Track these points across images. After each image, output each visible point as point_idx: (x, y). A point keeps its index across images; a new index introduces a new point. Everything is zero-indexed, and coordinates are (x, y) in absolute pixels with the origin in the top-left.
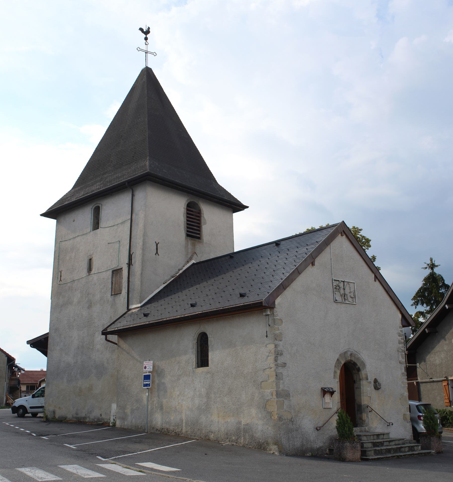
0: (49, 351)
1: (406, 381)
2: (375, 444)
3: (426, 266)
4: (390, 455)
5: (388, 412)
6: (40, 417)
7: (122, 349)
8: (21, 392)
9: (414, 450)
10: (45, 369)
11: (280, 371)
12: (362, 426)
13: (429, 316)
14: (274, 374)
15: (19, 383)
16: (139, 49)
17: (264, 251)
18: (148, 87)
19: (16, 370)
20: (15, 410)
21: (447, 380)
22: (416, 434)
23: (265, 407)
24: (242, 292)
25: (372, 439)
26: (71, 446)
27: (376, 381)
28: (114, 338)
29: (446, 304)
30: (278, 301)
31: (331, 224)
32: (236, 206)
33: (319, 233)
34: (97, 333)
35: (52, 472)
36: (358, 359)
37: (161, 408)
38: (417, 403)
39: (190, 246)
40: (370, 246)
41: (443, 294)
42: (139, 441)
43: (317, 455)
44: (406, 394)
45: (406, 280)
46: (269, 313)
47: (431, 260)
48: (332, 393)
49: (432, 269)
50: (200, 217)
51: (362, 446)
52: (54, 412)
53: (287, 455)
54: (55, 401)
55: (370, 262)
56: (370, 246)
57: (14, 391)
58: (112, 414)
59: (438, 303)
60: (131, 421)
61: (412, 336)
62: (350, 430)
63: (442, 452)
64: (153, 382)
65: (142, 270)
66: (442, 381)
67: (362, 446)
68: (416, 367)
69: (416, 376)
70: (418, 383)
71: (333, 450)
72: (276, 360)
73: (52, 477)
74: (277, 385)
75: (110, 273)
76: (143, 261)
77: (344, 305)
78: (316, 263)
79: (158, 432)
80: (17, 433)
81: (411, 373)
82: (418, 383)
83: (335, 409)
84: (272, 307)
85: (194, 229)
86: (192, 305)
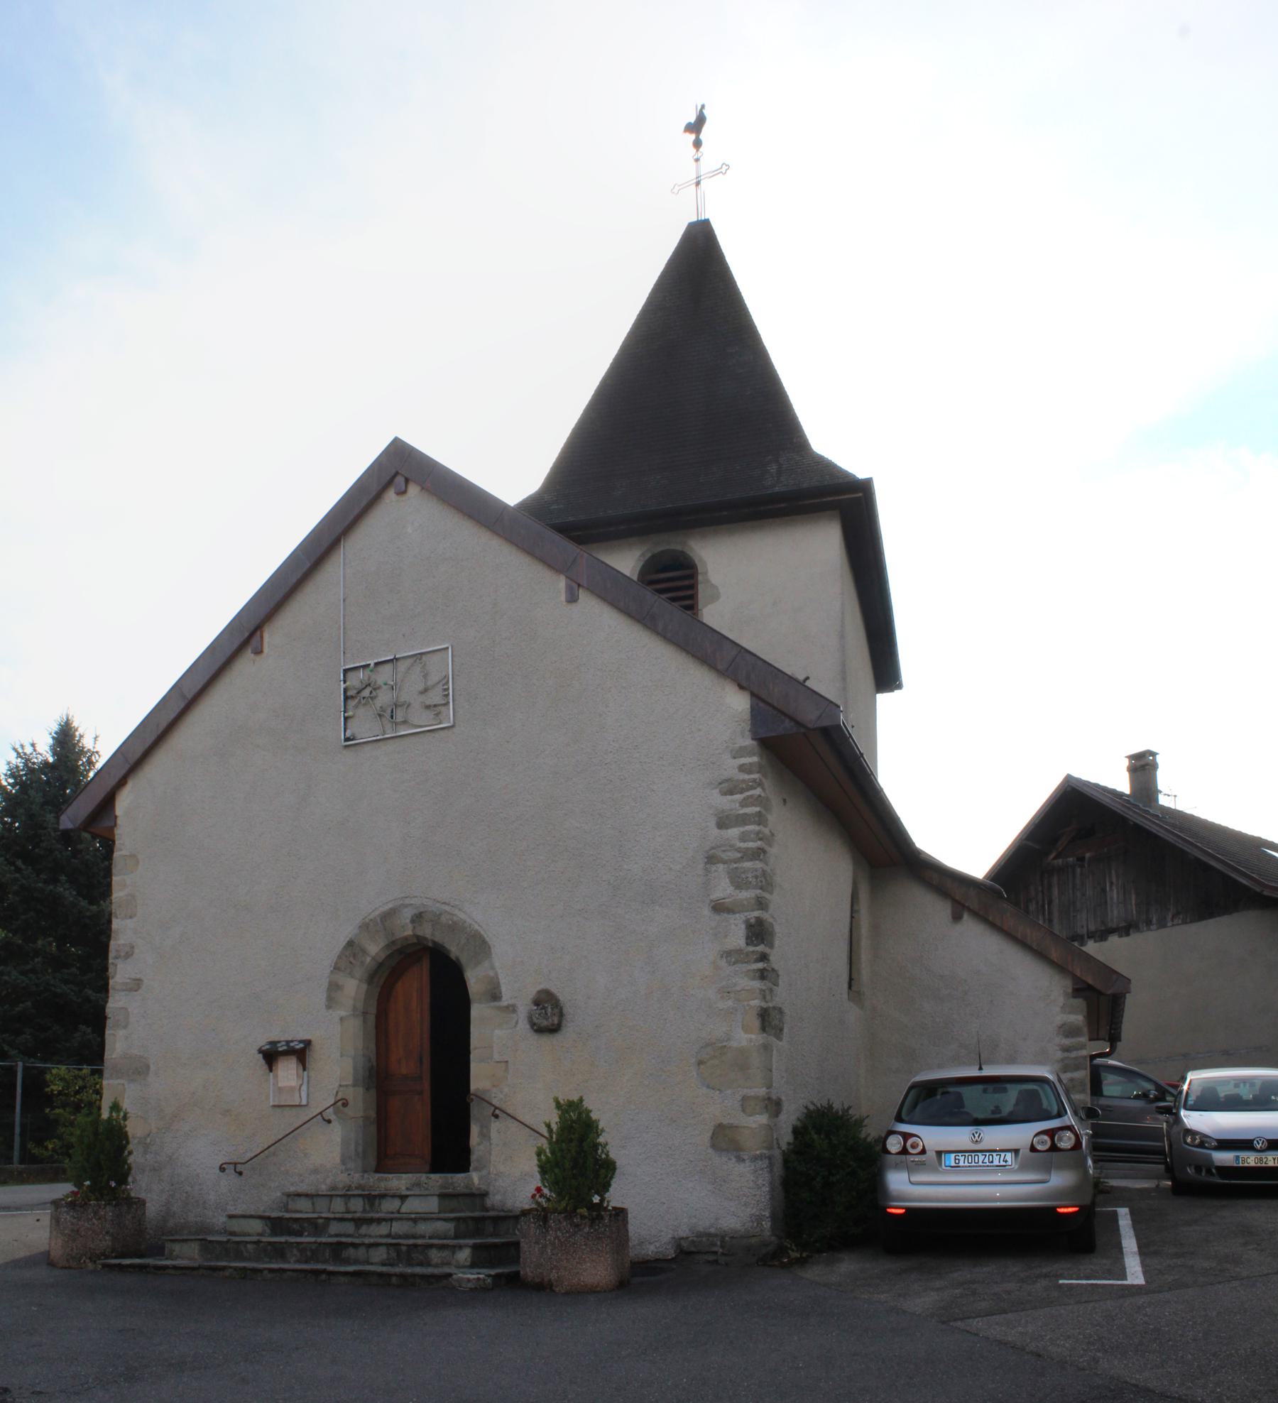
11: (120, 1004)
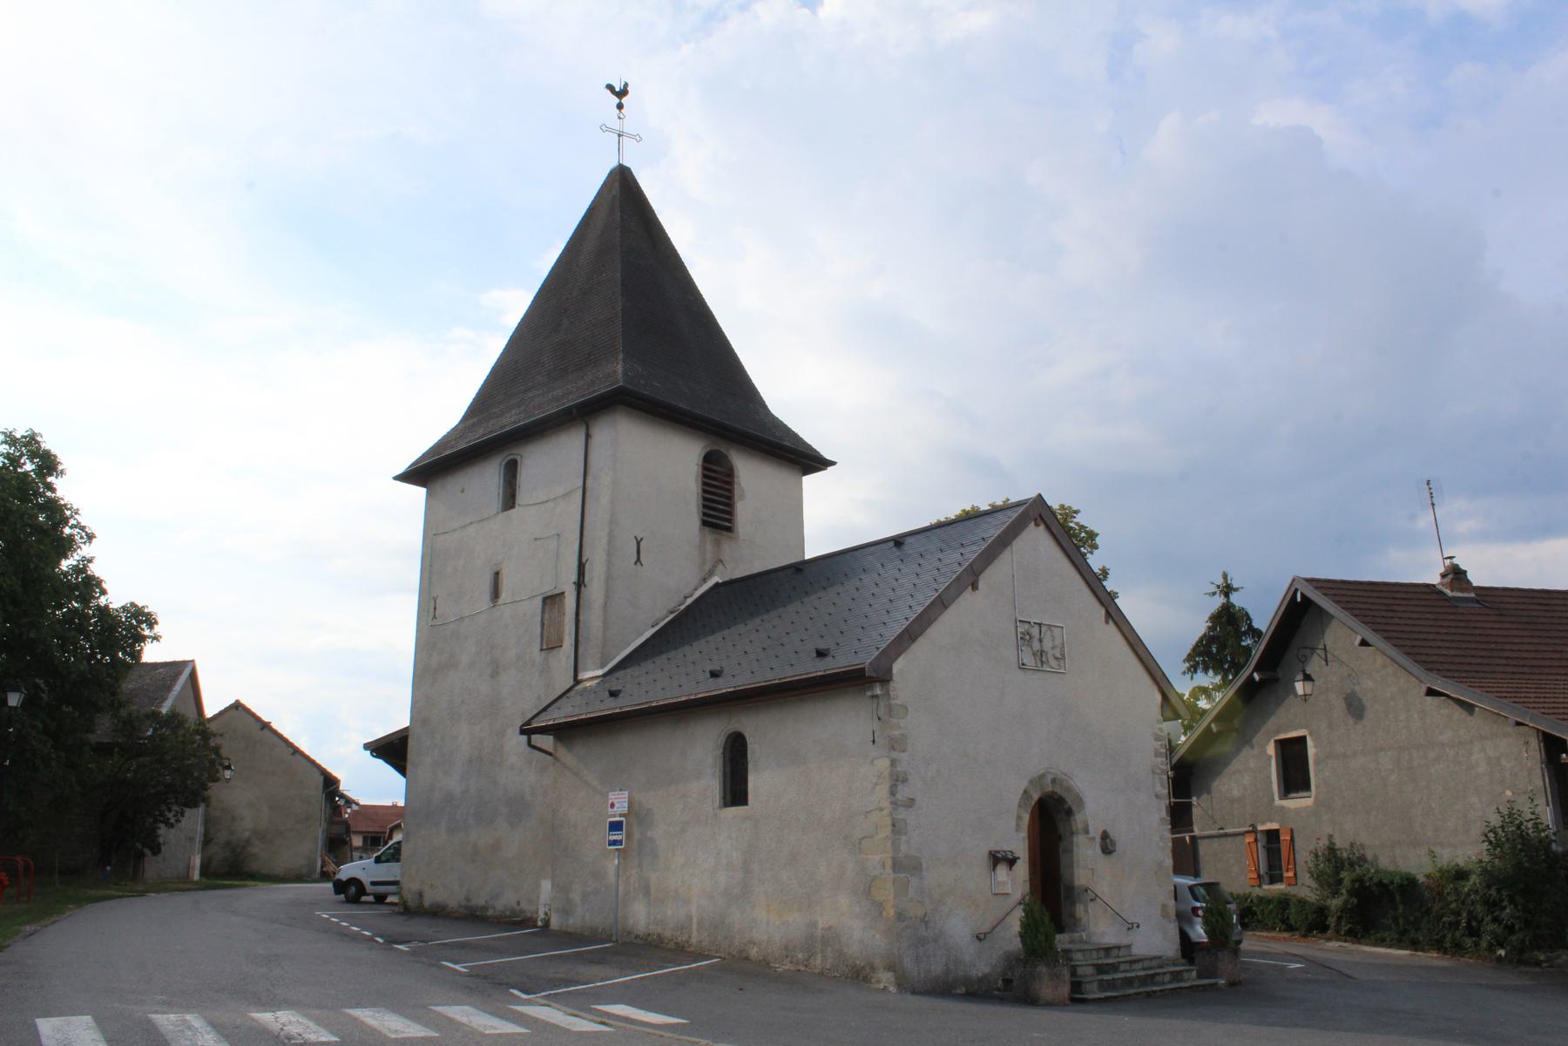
0: (409, 767)
1: (1169, 836)
2: (1100, 969)
3: (1213, 589)
4: (1132, 991)
5: (1130, 904)
6: (392, 904)
7: (564, 765)
8: (353, 849)
9: (1182, 980)
10: (401, 803)
12: (1073, 931)
13: (1218, 696)
14: (888, 821)
15: (348, 831)
16: (605, 128)
17: (871, 558)
18: (622, 203)
19: (342, 802)
20: (341, 887)
21: (1254, 831)
22: (1188, 947)
23: (868, 892)
24: (822, 646)
25: (1095, 959)
26: (457, 967)
27: (1105, 836)
28: (546, 741)
29: (1256, 669)
30: (898, 667)
31: (1013, 500)
32: (808, 461)
33: (988, 519)
34: (510, 731)
35: (417, 1019)
36: (1069, 789)
37: (647, 891)
38: (1190, 881)
39: (709, 547)
40: (1095, 547)
41: (1248, 650)
42: (599, 959)
43: (978, 991)
44: (1169, 862)
45: (1169, 619)
46: (878, 692)
47: (1225, 576)
48: (1012, 862)
49: (1227, 595)
50: (731, 483)
51: (1073, 973)
52: (421, 895)
53: (914, 992)
54: (428, 871)
55: (1095, 582)
56: (1095, 547)
57: (337, 846)
58: (542, 901)
59: (1237, 668)
60: (582, 917)
61: (1183, 738)
62: (1049, 940)
63: (1240, 983)
64: (629, 836)
65: (607, 596)
66: (1243, 834)
67: (1073, 973)
68: (1189, 805)
69: (1191, 824)
70: (1193, 839)
71: (1011, 981)
72: (893, 793)
73: (415, 1031)
74: (895, 846)
75: (538, 602)
76: (609, 578)
77: (1039, 675)
78: (981, 584)
79: (639, 941)
80: (346, 935)
81: (1180, 816)
82: (1193, 839)
83: (1018, 896)
84: (885, 678)
85: (718, 508)
86: (714, 674)
